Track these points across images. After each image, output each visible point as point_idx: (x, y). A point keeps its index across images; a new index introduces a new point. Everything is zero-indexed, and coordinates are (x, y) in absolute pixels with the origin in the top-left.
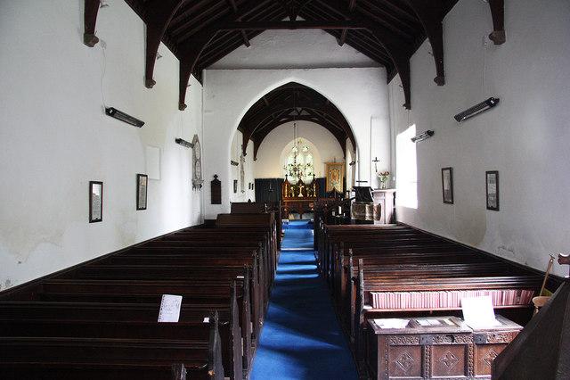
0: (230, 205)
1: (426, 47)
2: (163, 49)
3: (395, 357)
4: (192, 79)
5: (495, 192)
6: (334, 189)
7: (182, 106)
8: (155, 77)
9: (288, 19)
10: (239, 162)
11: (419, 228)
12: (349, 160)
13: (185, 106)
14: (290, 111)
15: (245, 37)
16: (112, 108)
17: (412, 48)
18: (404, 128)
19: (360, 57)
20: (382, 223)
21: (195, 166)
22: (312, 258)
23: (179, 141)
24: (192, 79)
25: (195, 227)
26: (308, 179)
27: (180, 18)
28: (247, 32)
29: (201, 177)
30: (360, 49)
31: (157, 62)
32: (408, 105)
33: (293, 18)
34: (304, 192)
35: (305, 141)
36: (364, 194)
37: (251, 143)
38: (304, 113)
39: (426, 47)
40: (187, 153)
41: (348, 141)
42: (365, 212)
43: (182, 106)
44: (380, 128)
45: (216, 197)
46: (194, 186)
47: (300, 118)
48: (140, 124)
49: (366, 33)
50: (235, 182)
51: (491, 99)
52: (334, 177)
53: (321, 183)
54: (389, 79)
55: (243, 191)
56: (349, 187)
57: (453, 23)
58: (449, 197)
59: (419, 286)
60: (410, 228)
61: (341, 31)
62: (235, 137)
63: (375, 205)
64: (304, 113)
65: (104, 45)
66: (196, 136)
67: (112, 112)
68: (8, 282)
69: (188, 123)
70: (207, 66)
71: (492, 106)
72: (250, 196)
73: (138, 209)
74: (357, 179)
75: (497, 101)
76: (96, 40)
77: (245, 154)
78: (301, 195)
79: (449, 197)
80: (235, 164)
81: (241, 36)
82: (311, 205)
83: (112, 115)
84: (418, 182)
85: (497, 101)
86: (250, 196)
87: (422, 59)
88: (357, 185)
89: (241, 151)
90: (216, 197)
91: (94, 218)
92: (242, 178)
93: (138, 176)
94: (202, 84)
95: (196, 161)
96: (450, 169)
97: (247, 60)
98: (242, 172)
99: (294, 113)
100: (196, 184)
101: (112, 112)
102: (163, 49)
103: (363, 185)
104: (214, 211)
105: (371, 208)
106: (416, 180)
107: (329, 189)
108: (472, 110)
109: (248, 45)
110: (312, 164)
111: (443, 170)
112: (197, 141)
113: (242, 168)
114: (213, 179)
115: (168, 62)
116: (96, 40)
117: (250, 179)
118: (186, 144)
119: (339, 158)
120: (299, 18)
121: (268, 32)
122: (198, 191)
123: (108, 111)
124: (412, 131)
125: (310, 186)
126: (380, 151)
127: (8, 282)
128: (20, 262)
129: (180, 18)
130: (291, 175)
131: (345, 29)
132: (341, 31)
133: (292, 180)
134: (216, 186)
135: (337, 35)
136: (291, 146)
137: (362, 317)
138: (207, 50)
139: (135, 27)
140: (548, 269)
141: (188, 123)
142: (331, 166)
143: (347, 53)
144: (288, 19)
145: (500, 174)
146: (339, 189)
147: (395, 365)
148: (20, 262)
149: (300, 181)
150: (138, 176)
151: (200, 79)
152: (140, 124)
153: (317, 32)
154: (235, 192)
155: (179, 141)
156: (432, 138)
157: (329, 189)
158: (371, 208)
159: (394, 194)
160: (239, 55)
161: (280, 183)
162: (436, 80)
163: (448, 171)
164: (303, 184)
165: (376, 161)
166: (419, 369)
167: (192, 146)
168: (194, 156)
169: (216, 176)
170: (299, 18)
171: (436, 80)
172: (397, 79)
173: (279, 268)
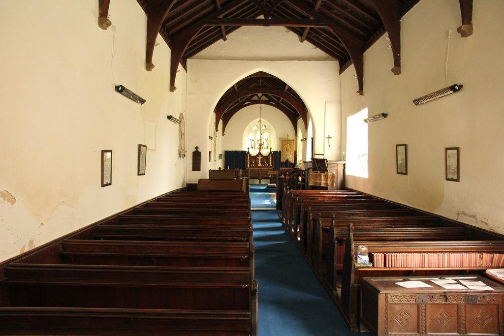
0: (208, 171)
2: (159, 39)
4: (180, 67)
5: (455, 165)
6: (287, 160)
7: (172, 88)
10: (213, 136)
11: (371, 194)
12: (300, 136)
13: (175, 88)
14: (253, 96)
15: (224, 32)
16: (121, 86)
17: (367, 41)
18: (356, 110)
19: (319, 52)
22: (277, 217)
23: (170, 118)
25: (179, 190)
26: (265, 152)
27: (173, 12)
28: (226, 28)
30: (317, 45)
31: (155, 48)
32: (361, 91)
34: (263, 163)
36: (320, 165)
37: (221, 122)
38: (264, 98)
39: (383, 42)
40: (174, 127)
41: (300, 122)
42: (321, 179)
43: (172, 88)
44: (332, 112)
45: (196, 166)
46: (180, 156)
48: (142, 101)
49: (326, 31)
50: (210, 153)
51: (455, 85)
52: (287, 150)
53: (276, 155)
54: (341, 71)
55: (215, 161)
57: (410, 21)
58: (403, 170)
59: (402, 249)
60: (360, 193)
61: (303, 29)
62: (212, 116)
63: (329, 174)
64: (264, 98)
65: (114, 29)
66: (181, 114)
67: (120, 89)
68: (31, 242)
69: (175, 103)
70: (190, 56)
71: (455, 91)
72: (218, 164)
73: (139, 174)
75: (461, 87)
76: (109, 24)
77: (217, 130)
78: (260, 165)
79: (403, 170)
80: (211, 138)
81: (220, 31)
82: (269, 173)
83: (120, 92)
84: (369, 154)
85: (461, 87)
86: (218, 164)
89: (214, 128)
90: (196, 166)
91: (105, 183)
92: (215, 149)
93: (140, 146)
94: (186, 70)
95: (182, 135)
97: (224, 53)
98: (215, 145)
99: (255, 98)
100: (182, 155)
101: (120, 89)
102: (159, 39)
103: (321, 157)
104: (195, 177)
105: (326, 177)
106: (366, 152)
107: (283, 160)
108: (431, 96)
109: (225, 40)
112: (183, 118)
113: (215, 141)
114: (194, 150)
115: (162, 50)
116: (109, 24)
117: (220, 151)
118: (175, 121)
119: (291, 136)
121: (244, 28)
122: (182, 160)
123: (117, 88)
124: (364, 113)
125: (266, 158)
126: (332, 129)
127: (31, 242)
128: (42, 224)
129: (178, 9)
130: (252, 148)
131: (308, 27)
132: (303, 29)
134: (197, 156)
135: (300, 32)
136: (254, 124)
138: (193, 42)
139: (140, 17)
141: (175, 103)
142: (284, 141)
143: (308, 48)
144: (262, 17)
145: (461, 150)
146: (292, 160)
148: (42, 224)
149: (260, 153)
150: (140, 146)
151: (185, 67)
152: (142, 101)
153: (282, 29)
155: (170, 118)
157: (283, 160)
158: (326, 177)
159: (344, 165)
160: (217, 47)
161: (243, 155)
162: (393, 70)
164: (262, 156)
165: (329, 138)
166: (415, 325)
167: (180, 122)
168: (180, 130)
169: (197, 148)
171: (393, 70)
172: (351, 69)
173: (255, 226)
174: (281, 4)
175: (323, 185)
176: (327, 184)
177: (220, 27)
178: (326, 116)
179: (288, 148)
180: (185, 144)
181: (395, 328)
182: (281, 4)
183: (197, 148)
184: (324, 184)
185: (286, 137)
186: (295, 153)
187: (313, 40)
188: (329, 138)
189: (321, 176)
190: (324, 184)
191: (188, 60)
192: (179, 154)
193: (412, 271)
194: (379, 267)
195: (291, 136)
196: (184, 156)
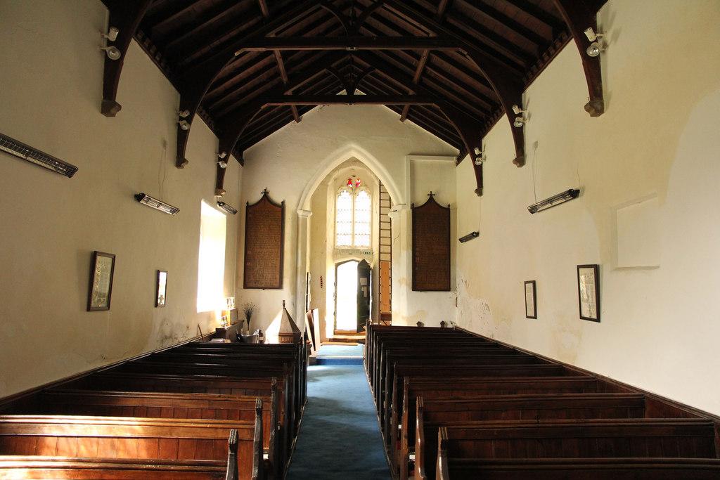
1: (571, 48)
8: (187, 156)
9: (344, 92)
15: (295, 112)
24: (232, 165)
33: (351, 91)
35: (376, 168)
39: (569, 58)
61: (403, 106)
87: (498, 138)
96: (534, 283)
109: (298, 121)
111: (526, 283)
115: (201, 135)
120: (358, 92)
131: (407, 105)
140: (319, 362)
144: (344, 92)
156: (576, 200)
163: (531, 285)
170: (358, 92)
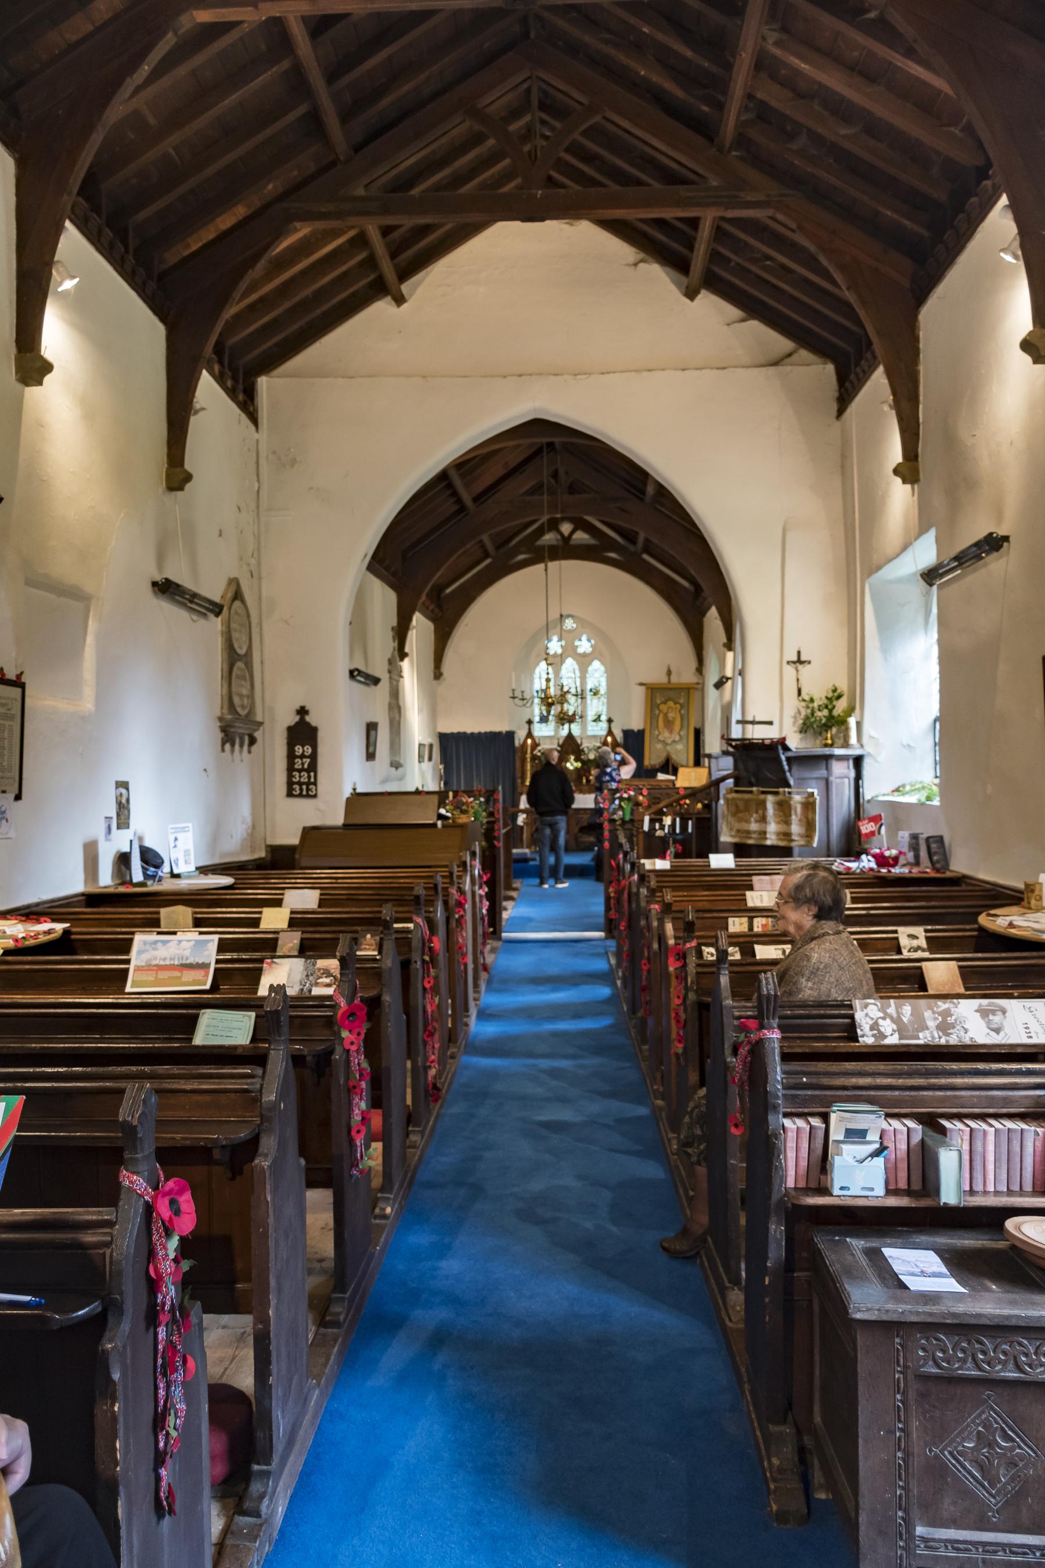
3: (939, 1434)
20: (593, 863)
21: (229, 675)
29: (251, 712)
37: (421, 626)
42: (763, 819)
47: (566, 551)
50: (371, 728)
56: (713, 744)
64: (581, 537)
74: (736, 715)
88: (736, 732)
89: (392, 645)
94: (254, 418)
102: (418, 619)
103: (757, 733)
108: (409, 1043)
109: (400, 300)
110: (603, 690)
114: (294, 719)
122: (242, 760)
132: (694, 223)
133: (549, 734)
137: (777, 1230)
147: (938, 1471)
154: (370, 756)
158: (784, 809)
165: (799, 661)
169: (302, 711)
173: (490, 999)
174: (584, 134)
175: (771, 840)
176: (787, 835)
177: (361, 241)
178: (787, 569)
179: (671, 715)
180: (251, 696)
181: (948, 1506)
182: (584, 134)
183: (302, 711)
184: (778, 834)
185: (660, 678)
186: (698, 734)
187: (733, 286)
188: (799, 661)
189: (763, 804)
190: (778, 834)
191: (263, 382)
192: (223, 729)
193: (468, 1016)
194: (985, 1193)
195: (686, 675)
196: (253, 741)
